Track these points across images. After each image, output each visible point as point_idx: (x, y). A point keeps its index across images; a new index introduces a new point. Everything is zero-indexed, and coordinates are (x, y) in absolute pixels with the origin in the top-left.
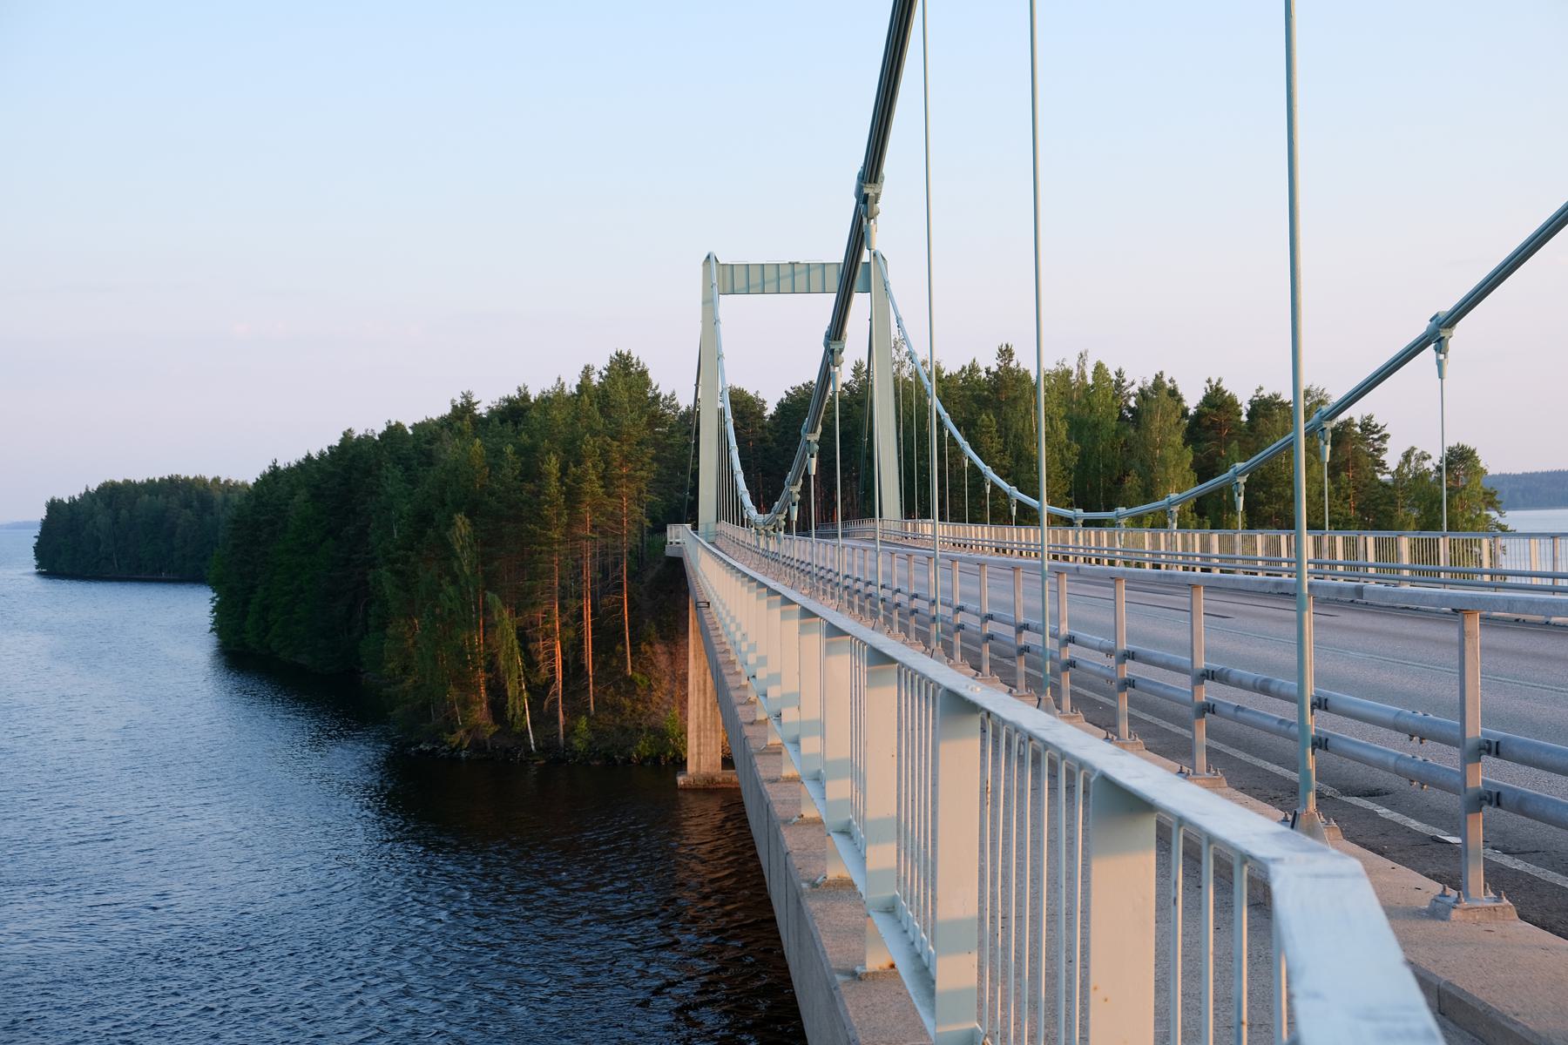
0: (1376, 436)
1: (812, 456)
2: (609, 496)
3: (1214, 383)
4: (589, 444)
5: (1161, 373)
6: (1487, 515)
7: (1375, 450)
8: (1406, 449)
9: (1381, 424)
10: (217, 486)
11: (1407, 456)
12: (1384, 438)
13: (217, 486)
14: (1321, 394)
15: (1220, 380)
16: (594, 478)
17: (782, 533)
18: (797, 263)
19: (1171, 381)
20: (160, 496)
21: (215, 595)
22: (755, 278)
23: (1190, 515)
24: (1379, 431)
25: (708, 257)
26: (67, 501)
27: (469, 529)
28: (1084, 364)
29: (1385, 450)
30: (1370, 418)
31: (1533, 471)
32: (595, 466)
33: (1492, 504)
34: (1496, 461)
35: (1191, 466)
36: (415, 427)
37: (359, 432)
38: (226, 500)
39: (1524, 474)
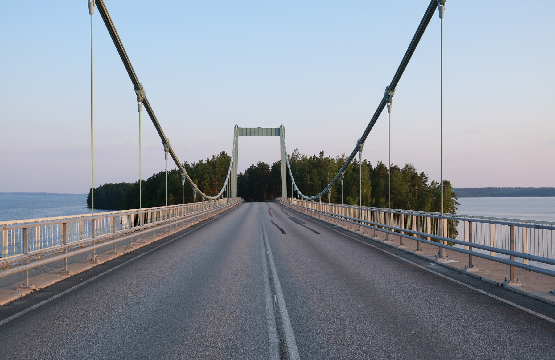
0: (425, 177)
1: (183, 180)
2: (212, 190)
3: (380, 162)
4: (206, 175)
5: (366, 159)
6: (452, 199)
7: (425, 181)
8: (432, 181)
9: (426, 174)
11: (432, 183)
12: (427, 178)
14: (411, 166)
15: (381, 162)
16: (208, 185)
17: (320, 202)
18: (260, 128)
19: (369, 162)
20: (119, 188)
23: (369, 198)
24: (425, 176)
25: (281, 126)
27: (173, 198)
28: (344, 157)
29: (427, 181)
30: (423, 172)
31: (483, 187)
32: (208, 182)
33: (453, 196)
34: (455, 185)
35: (370, 184)
39: (480, 188)
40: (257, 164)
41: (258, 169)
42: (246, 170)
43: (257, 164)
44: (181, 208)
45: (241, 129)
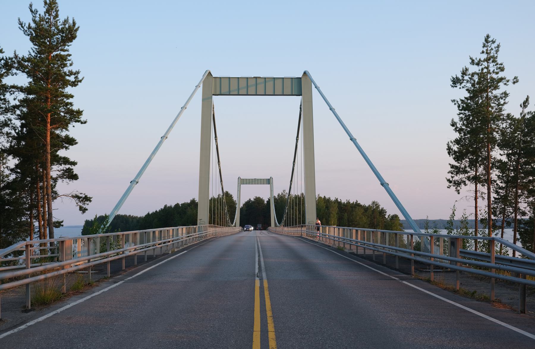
10: (129, 217)
13: (129, 217)
21: (8, 148)
22: (248, 182)
26: (90, 220)
30: (383, 208)
36: (182, 204)
37: (168, 205)
38: (132, 221)
40: (254, 199)
41: (254, 203)
42: (244, 203)
43: (254, 199)
44: (178, 229)
45: (243, 180)
